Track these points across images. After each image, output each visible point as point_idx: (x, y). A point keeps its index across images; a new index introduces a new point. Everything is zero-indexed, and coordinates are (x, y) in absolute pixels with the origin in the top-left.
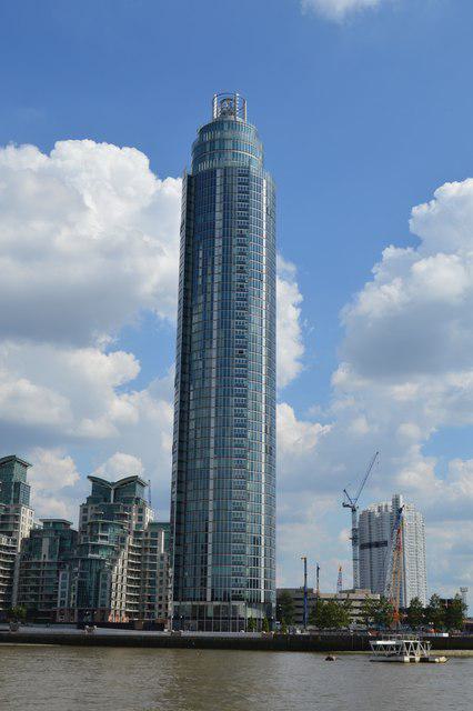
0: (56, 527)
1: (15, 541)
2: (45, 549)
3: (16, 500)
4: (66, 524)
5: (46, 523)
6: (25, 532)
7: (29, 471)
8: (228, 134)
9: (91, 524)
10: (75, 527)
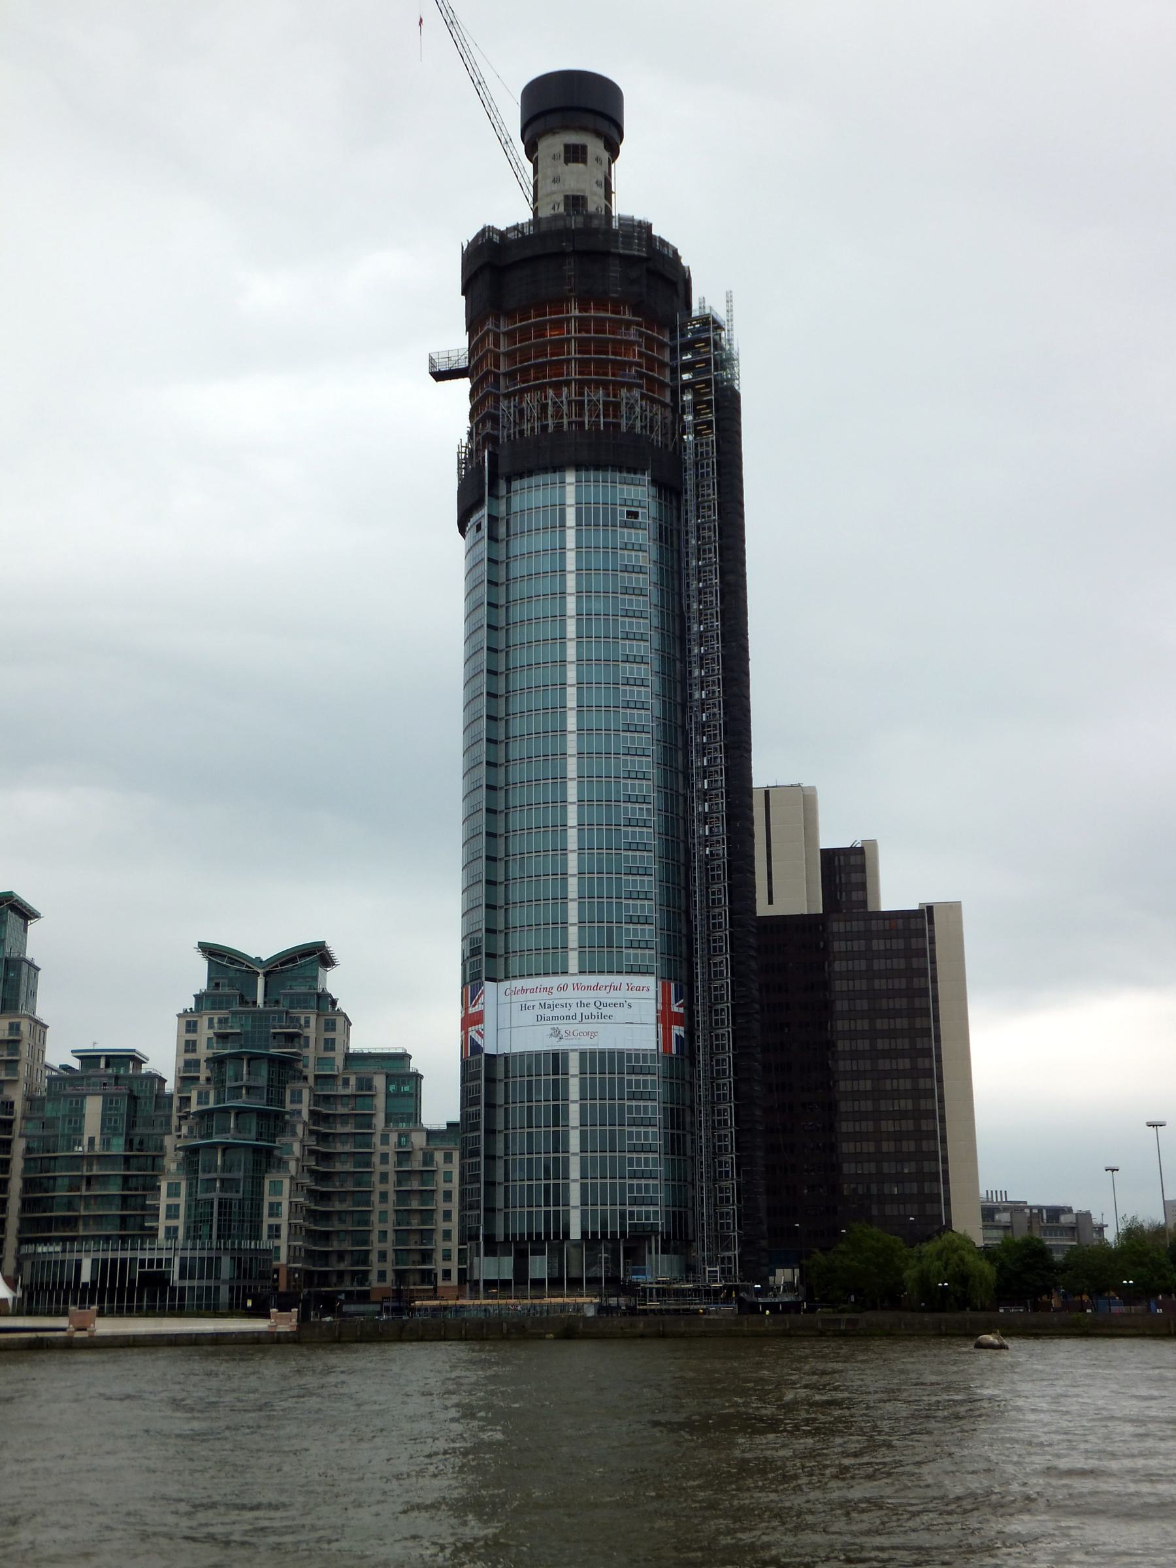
0: (114, 1070)
7: (33, 927)
10: (162, 1058)
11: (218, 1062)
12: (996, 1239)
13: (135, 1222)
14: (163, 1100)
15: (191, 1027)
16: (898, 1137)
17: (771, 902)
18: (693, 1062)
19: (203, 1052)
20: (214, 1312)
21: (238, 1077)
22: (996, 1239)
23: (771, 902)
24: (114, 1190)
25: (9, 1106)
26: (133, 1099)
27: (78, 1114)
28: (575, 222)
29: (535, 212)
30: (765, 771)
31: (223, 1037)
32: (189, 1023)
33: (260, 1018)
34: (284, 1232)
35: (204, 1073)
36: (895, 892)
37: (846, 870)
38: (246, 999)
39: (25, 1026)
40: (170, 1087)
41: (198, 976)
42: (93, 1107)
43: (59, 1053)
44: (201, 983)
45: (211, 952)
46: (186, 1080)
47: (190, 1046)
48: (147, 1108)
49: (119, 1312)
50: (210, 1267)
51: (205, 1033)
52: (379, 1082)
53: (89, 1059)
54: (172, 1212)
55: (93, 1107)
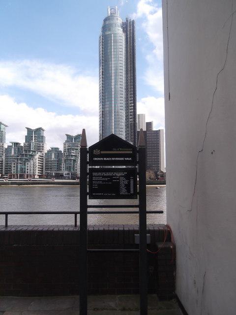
0: (56, 150)
1: (43, 154)
2: (53, 156)
3: (42, 142)
4: (58, 149)
5: (52, 148)
6: (45, 151)
7: (44, 132)
8: (112, 22)
9: (68, 149)
10: (61, 149)
13: (59, 168)
14: (61, 154)
15: (65, 145)
16: (154, 159)
17: (162, 212)
19: (67, 148)
20: (69, 179)
23: (162, 212)
24: (56, 164)
26: (18, 149)
28: (149, 174)
30: (138, 112)
33: (73, 144)
36: (155, 129)
37: (149, 125)
40: (62, 152)
41: (66, 138)
45: (66, 135)
47: (65, 147)
48: (20, 149)
49: (57, 179)
50: (68, 174)
54: (14, 167)
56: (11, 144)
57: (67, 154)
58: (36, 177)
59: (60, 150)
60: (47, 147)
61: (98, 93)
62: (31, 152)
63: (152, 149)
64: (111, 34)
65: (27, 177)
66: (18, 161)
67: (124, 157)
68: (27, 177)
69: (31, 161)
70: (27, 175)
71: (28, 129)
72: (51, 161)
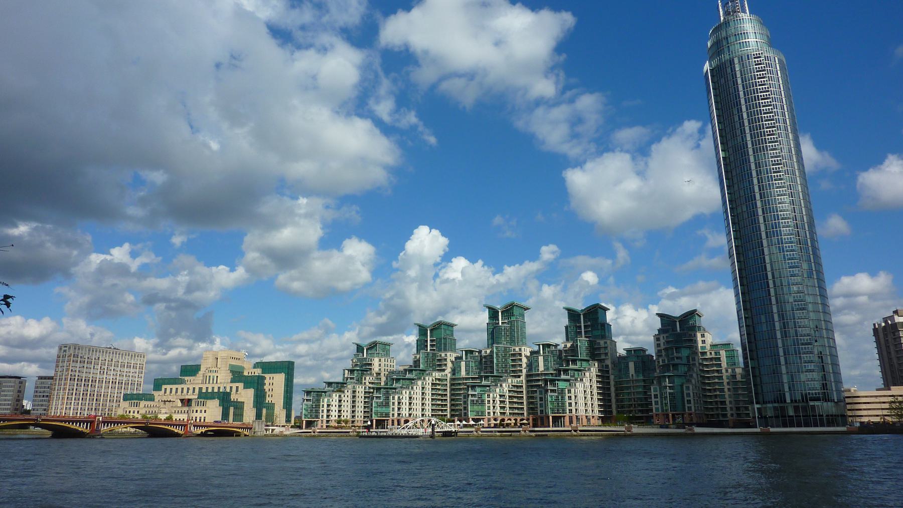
0: (637, 354)
4: (644, 351)
10: (652, 351)
11: (666, 349)
12: (7, 409)
15: (658, 339)
18: (22, 414)
19: (662, 347)
21: (673, 354)
22: (7, 409)
25: (607, 366)
26: (643, 362)
27: (627, 367)
29: (627, 152)
31: (668, 342)
32: (657, 339)
34: (692, 402)
35: (663, 353)
38: (674, 329)
39: (608, 342)
42: (631, 365)
43: (621, 350)
44: (659, 326)
46: (659, 353)
47: (658, 345)
51: (662, 341)
52: (723, 353)
53: (629, 351)
55: (631, 365)
56: (536, 348)
57: (663, 361)
58: (592, 421)
59: (647, 353)
60: (463, 343)
61: (824, 272)
62: (579, 363)
63: (716, 402)
64: (731, 62)
65: (571, 422)
66: (546, 384)
67: (799, 169)
68: (571, 422)
69: (577, 384)
70: (571, 418)
71: (489, 308)
72: (628, 382)
